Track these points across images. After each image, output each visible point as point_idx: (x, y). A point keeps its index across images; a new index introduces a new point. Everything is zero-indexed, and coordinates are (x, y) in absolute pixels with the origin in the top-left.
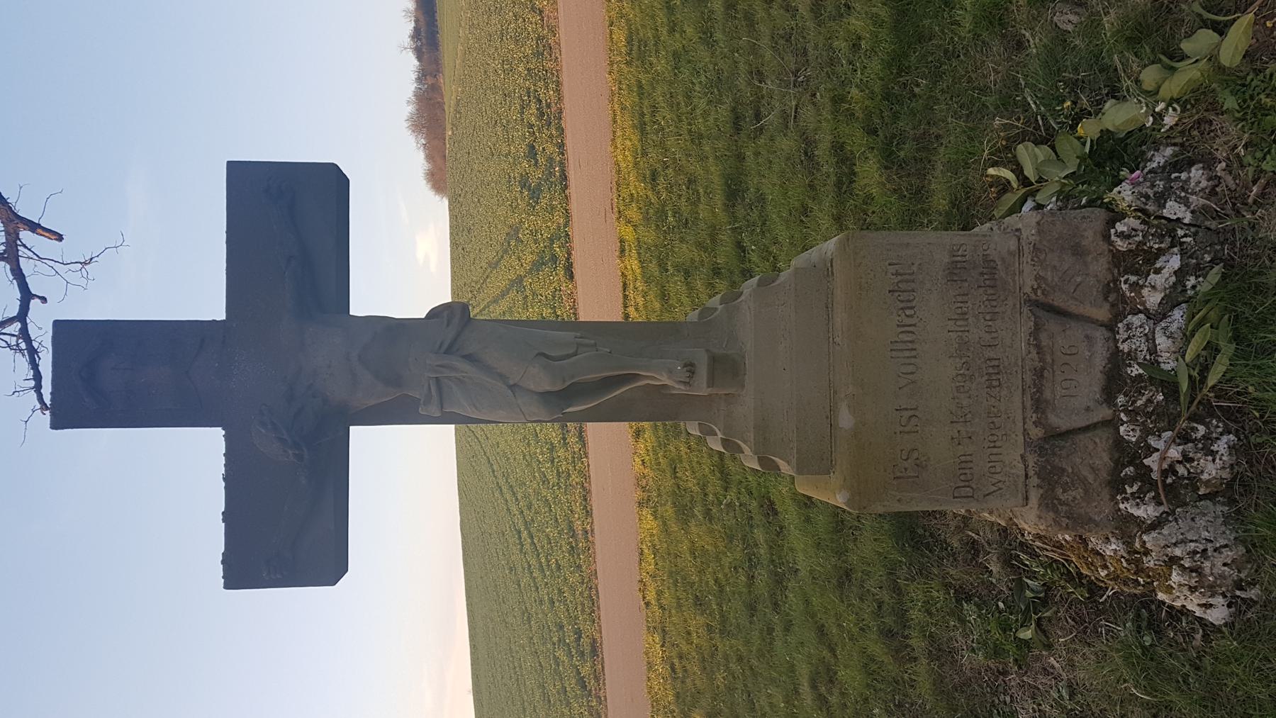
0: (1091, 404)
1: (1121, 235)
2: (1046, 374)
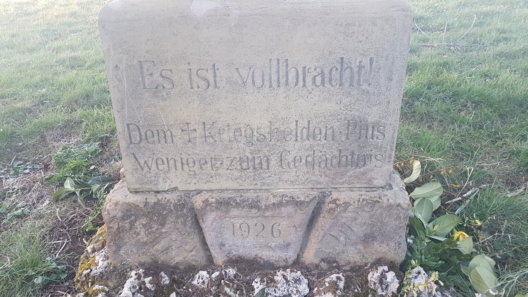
0: (227, 248)
1: (383, 276)
2: (254, 211)
